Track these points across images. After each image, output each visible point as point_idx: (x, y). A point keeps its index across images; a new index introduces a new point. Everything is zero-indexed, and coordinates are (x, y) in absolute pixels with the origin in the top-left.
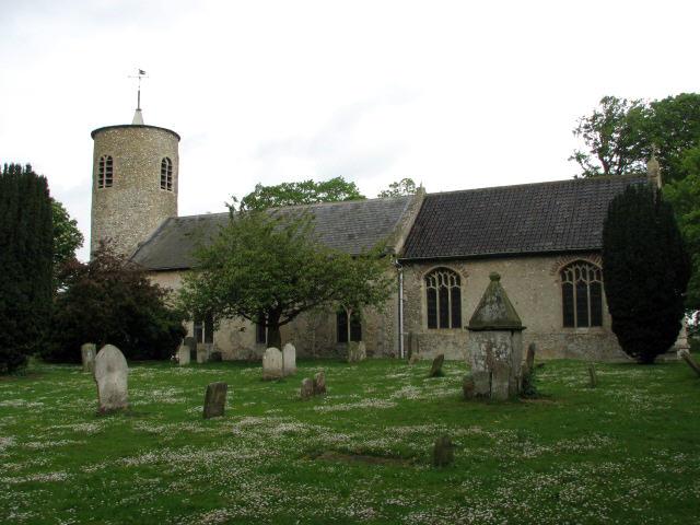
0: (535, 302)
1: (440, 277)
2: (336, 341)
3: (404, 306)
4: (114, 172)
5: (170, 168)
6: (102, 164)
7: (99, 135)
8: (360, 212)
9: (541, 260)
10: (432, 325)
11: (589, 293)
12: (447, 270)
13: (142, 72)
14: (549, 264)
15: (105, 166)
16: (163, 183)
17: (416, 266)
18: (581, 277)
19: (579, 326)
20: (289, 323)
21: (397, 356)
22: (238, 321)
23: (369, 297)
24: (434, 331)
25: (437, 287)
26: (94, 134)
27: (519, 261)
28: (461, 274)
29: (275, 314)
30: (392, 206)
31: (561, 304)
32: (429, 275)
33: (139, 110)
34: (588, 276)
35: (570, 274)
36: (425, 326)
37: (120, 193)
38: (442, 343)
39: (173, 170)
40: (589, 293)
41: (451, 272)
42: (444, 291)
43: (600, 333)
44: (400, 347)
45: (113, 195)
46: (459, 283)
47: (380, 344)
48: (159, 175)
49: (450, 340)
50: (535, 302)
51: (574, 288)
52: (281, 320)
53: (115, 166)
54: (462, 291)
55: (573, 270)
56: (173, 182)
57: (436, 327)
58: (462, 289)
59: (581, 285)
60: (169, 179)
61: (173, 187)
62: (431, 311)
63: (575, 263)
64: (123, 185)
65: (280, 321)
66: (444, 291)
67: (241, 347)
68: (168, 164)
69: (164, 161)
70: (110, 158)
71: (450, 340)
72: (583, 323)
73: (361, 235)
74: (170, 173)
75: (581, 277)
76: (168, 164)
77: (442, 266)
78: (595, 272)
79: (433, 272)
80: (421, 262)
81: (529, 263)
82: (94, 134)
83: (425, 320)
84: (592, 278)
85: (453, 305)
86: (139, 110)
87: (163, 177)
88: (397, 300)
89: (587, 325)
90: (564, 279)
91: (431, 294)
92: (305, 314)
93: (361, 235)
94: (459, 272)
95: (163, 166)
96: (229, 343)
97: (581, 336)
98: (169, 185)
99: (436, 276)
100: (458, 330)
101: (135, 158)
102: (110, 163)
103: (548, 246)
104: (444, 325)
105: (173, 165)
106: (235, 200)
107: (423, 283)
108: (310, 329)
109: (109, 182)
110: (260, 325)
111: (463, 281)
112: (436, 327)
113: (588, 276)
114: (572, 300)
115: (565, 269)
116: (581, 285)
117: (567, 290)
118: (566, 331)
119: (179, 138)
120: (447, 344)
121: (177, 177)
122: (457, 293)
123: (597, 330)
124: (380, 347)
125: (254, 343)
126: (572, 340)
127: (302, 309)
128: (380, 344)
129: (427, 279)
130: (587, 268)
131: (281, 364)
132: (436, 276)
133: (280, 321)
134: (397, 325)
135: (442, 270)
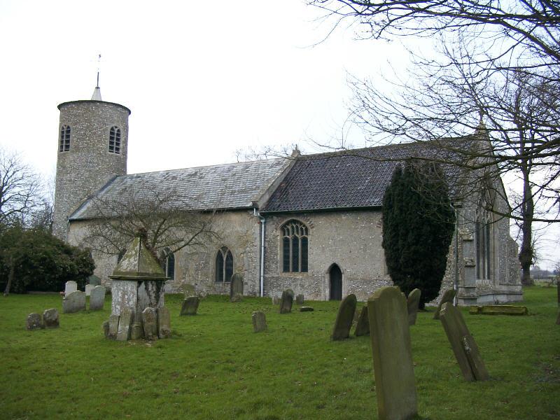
0: (365, 251)
1: (293, 227)
4: (71, 139)
6: (63, 132)
9: (371, 214)
10: (286, 269)
12: (298, 222)
16: (111, 148)
17: (275, 218)
21: (258, 295)
24: (286, 275)
26: (59, 107)
27: (354, 215)
33: (98, 88)
35: (288, 230)
36: (280, 269)
39: (122, 139)
41: (301, 224)
42: (295, 239)
45: (71, 156)
46: (307, 234)
48: (108, 141)
49: (299, 282)
50: (365, 251)
51: (300, 241)
53: (72, 135)
55: (289, 227)
56: (121, 146)
57: (289, 271)
58: (309, 238)
62: (286, 257)
64: (77, 149)
66: (295, 239)
69: (112, 129)
70: (68, 127)
75: (295, 233)
77: (294, 218)
78: (304, 228)
79: (288, 223)
80: (279, 214)
81: (364, 215)
82: (59, 107)
83: (280, 265)
85: (302, 251)
86: (98, 88)
87: (111, 143)
88: (258, 246)
91: (286, 241)
94: (307, 224)
98: (117, 149)
100: (305, 274)
101: (88, 127)
104: (295, 269)
107: (279, 233)
109: (67, 147)
111: (310, 232)
112: (289, 271)
114: (288, 257)
119: (130, 112)
121: (126, 142)
122: (305, 241)
129: (283, 229)
132: (289, 227)
134: (258, 268)
135: (294, 221)
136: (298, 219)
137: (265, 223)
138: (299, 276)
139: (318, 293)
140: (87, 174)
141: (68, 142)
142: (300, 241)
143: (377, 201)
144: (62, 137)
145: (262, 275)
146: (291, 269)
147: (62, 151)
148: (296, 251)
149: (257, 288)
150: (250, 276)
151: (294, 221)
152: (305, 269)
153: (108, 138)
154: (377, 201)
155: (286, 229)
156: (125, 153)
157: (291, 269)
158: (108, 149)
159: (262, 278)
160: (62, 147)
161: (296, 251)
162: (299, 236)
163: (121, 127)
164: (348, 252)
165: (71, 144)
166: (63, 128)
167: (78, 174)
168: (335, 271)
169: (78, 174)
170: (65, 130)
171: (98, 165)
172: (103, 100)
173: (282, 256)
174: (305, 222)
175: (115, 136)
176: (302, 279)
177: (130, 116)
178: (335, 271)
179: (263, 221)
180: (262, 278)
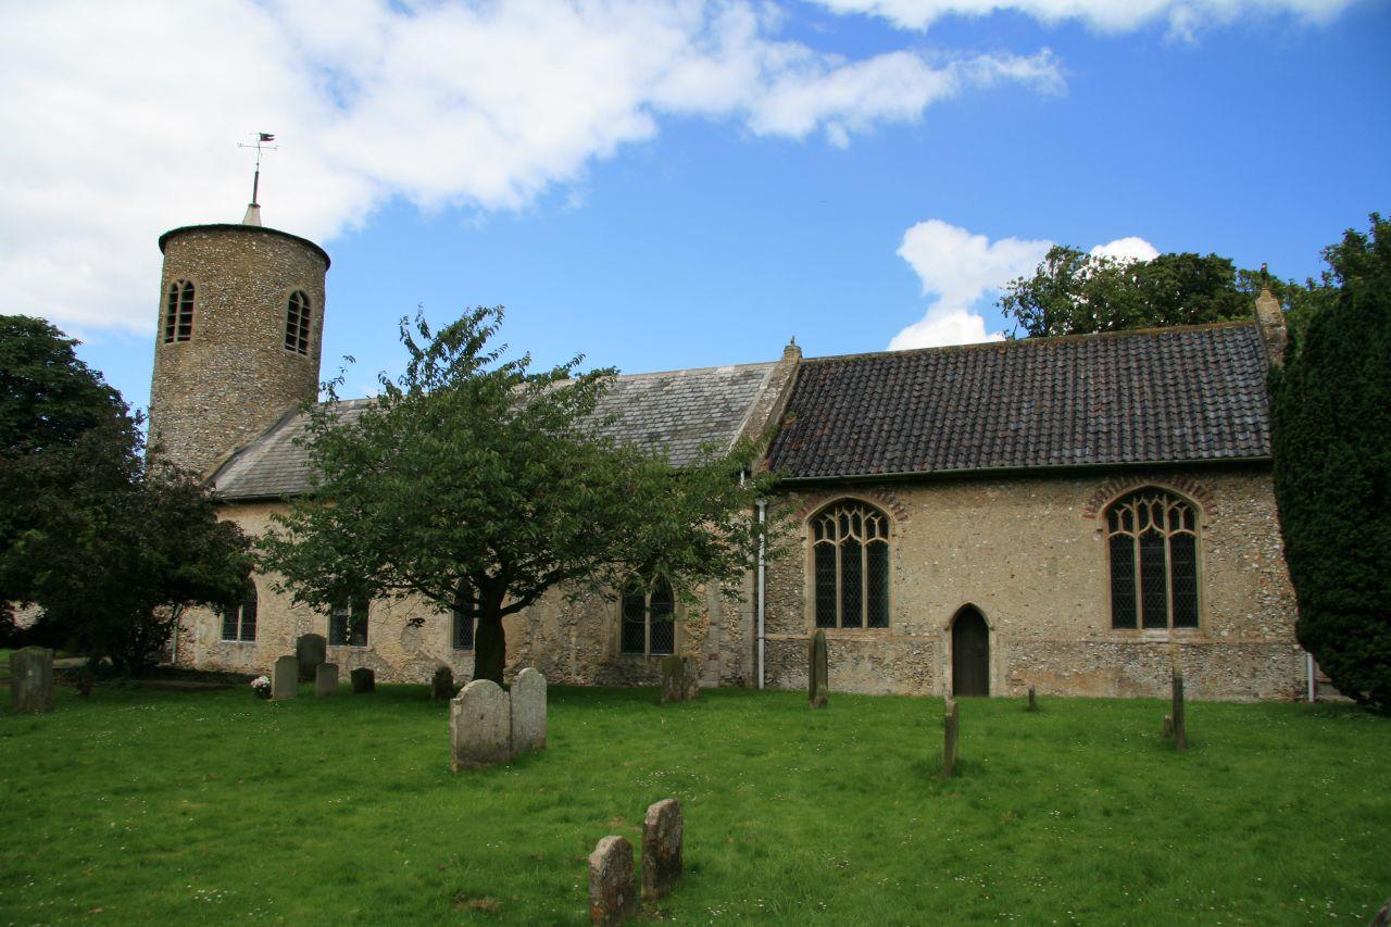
0: (1053, 573)
1: (844, 520)
2: (618, 649)
3: (767, 581)
4: (195, 312)
5: (306, 312)
6: (174, 297)
7: (170, 244)
8: (668, 392)
11: (1168, 557)
12: (859, 504)
13: (265, 137)
14: (1088, 491)
15: (180, 300)
16: (290, 340)
17: (793, 496)
18: (851, 532)
19: (1148, 624)
20: (523, 611)
22: (416, 604)
23: (707, 560)
25: (837, 542)
26: (164, 242)
28: (890, 514)
29: (494, 589)
30: (734, 382)
31: (1109, 577)
32: (821, 515)
33: (255, 206)
34: (1166, 521)
35: (831, 525)
37: (206, 352)
38: (849, 657)
40: (1168, 557)
41: (868, 508)
42: (851, 548)
43: (1197, 640)
44: (756, 665)
45: (193, 355)
46: (884, 533)
47: (713, 657)
48: (283, 323)
49: (867, 652)
50: (1053, 573)
51: (1167, 543)
52: (508, 600)
53: (199, 303)
54: (892, 549)
56: (311, 337)
57: (859, 624)
58: (893, 544)
59: (1152, 539)
60: (304, 333)
61: (309, 349)
63: (1138, 494)
64: (210, 336)
65: (503, 606)
66: (851, 548)
67: (422, 657)
68: (301, 303)
69: (294, 296)
70: (190, 285)
71: (867, 652)
72: (1155, 619)
73: (675, 433)
74: (305, 322)
76: (301, 303)
78: (876, 521)
79: (830, 509)
80: (803, 487)
81: (962, 495)
83: (810, 609)
84: (1174, 525)
86: (255, 206)
87: (291, 328)
89: (1162, 623)
90: (1113, 526)
91: (824, 555)
92: (554, 592)
93: (675, 433)
95: (293, 306)
96: (398, 648)
97: (1154, 647)
98: (303, 344)
99: (836, 519)
100: (883, 631)
102: (189, 295)
103: (1082, 457)
104: (852, 620)
105: (313, 309)
106: (424, 330)
107: (805, 531)
108: (566, 623)
109: (186, 330)
110: (462, 612)
112: (859, 624)
113: (1166, 521)
115: (1116, 505)
116: (1152, 539)
117: (1119, 551)
118: (1120, 636)
119: (328, 263)
120: (857, 660)
121: (319, 331)
122: (879, 553)
123: (1187, 634)
124: (714, 664)
125: (449, 650)
126: (1133, 656)
127: (554, 578)
128: (713, 657)
129: (816, 524)
130: (861, 514)
131: (506, 725)
132: (836, 519)
133: (503, 606)
136: (861, 497)
137: (766, 507)
138: (866, 635)
139: (923, 676)
140: (234, 397)
141: (186, 319)
142: (1167, 543)
143: (1254, 442)
144: (173, 308)
145: (761, 634)
146: (1170, 620)
147: (171, 340)
148: (851, 578)
149: (749, 666)
150: (728, 638)
151: (850, 504)
152: (879, 618)
153: (286, 316)
154: (1254, 442)
155: (824, 523)
156: (317, 357)
157: (1170, 620)
158: (283, 343)
159: (761, 642)
160: (170, 331)
161: (851, 578)
162: (863, 541)
163: (311, 295)
164: (1008, 576)
165: (195, 325)
166: (175, 288)
167: (211, 396)
168: (969, 626)
169: (211, 396)
170: (180, 292)
171: (262, 377)
172: (265, 224)
173: (814, 588)
174: (882, 507)
175: (300, 314)
176: (875, 645)
177: (329, 275)
178: (969, 626)
179: (761, 504)
180: (761, 642)
